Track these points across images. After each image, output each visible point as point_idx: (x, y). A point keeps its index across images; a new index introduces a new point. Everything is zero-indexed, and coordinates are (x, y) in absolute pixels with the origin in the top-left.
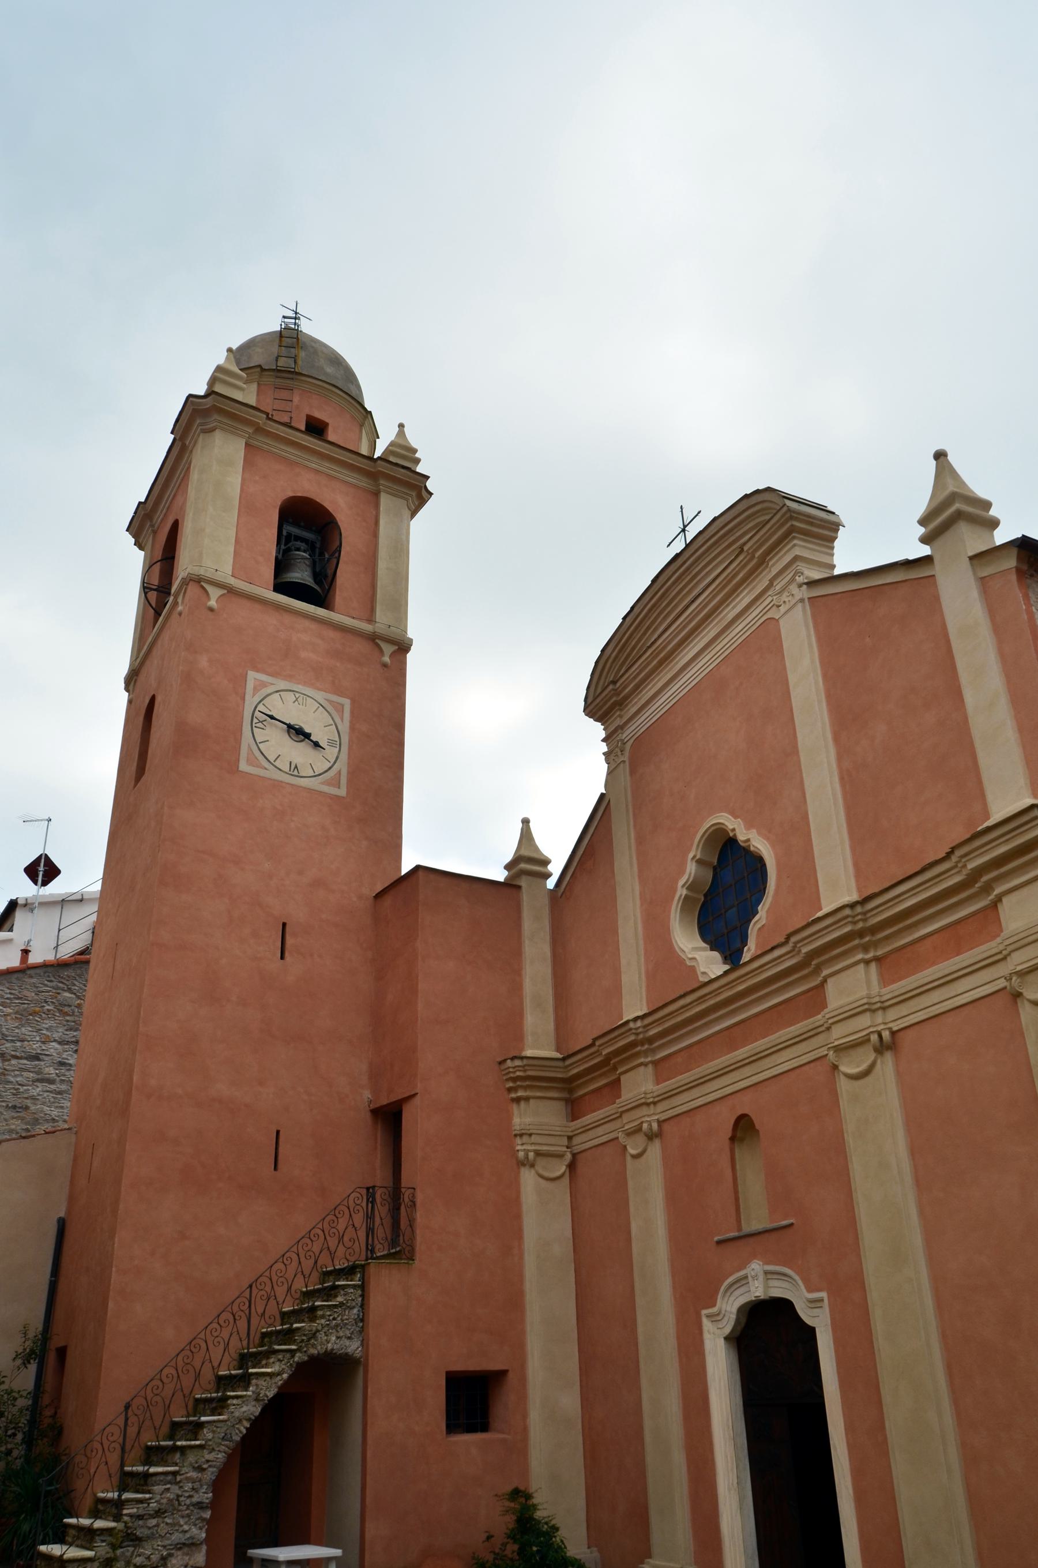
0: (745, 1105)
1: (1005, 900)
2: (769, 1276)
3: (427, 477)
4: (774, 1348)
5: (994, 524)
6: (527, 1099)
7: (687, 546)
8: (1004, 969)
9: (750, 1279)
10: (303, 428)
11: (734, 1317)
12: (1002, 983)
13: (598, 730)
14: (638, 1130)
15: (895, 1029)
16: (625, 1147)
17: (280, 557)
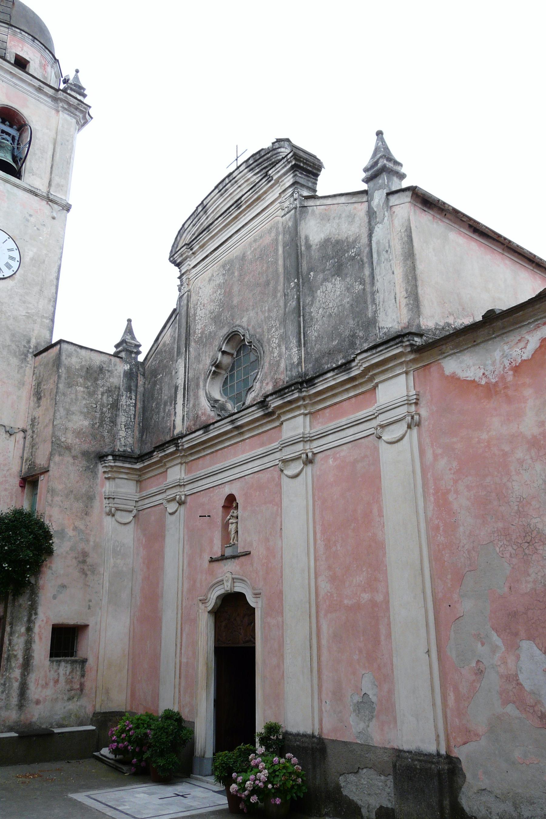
0: (234, 489)
1: (380, 386)
2: (235, 581)
4: (233, 616)
5: (402, 176)
6: (114, 479)
8: (374, 423)
9: (224, 581)
10: (13, 62)
11: (214, 601)
12: (372, 431)
14: (174, 499)
15: (315, 452)
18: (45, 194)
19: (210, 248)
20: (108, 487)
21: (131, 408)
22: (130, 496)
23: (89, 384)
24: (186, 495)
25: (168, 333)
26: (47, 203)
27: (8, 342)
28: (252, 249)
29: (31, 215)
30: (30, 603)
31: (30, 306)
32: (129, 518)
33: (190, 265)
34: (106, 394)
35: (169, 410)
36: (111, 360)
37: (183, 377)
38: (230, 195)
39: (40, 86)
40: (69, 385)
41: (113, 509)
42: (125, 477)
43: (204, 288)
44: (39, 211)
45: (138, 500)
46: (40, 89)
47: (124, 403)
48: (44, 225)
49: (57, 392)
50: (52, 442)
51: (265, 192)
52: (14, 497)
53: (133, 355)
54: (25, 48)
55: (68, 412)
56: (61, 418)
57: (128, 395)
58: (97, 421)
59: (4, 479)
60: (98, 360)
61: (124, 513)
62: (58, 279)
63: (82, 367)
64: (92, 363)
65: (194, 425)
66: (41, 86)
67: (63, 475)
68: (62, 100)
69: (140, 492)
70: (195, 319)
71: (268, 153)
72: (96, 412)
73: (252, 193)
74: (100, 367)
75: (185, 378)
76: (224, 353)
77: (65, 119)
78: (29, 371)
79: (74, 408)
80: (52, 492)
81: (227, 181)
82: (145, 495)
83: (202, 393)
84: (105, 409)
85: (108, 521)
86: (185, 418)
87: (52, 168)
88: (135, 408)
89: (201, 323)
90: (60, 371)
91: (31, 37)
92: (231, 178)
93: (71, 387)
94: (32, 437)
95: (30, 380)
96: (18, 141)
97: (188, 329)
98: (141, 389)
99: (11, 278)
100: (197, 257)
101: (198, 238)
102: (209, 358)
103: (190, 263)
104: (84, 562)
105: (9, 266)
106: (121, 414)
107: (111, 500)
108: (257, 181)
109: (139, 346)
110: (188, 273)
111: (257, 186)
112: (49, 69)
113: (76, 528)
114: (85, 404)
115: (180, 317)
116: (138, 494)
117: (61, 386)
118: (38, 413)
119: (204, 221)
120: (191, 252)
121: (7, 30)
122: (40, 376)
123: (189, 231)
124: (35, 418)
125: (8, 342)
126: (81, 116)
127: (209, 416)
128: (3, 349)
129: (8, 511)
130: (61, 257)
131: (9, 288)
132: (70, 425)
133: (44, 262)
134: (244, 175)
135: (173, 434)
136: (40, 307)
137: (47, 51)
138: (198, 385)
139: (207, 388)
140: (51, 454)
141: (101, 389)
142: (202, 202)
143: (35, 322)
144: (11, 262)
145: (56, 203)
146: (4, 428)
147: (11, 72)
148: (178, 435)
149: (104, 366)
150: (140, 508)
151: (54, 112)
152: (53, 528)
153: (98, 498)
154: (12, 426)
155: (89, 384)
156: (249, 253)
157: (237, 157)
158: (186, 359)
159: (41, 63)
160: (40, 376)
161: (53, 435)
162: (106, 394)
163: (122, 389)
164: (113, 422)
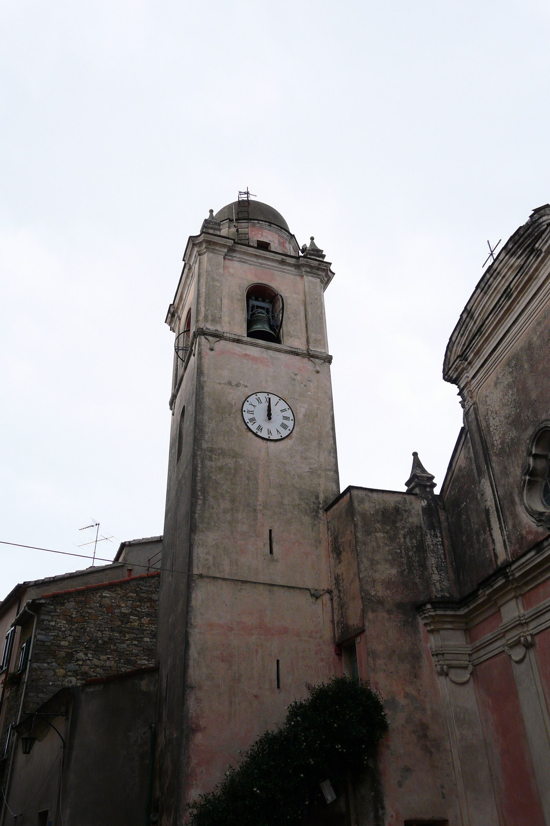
3: (330, 264)
6: (438, 630)
7: (495, 260)
10: (256, 246)
13: (455, 389)
14: (517, 643)
16: (510, 655)
17: (249, 318)
18: (305, 352)
19: (487, 352)
20: (433, 642)
21: (439, 547)
22: (461, 649)
23: (388, 528)
24: (532, 635)
25: (462, 455)
26: (309, 360)
27: (298, 502)
28: (538, 333)
29: (296, 374)
30: (373, 794)
31: (312, 461)
32: (465, 676)
33: (468, 377)
34: (408, 536)
35: (484, 540)
36: (405, 498)
37: (492, 497)
38: (495, 289)
39: (283, 259)
40: (368, 533)
41: (445, 667)
42: (450, 626)
43: (492, 395)
44: (302, 369)
45: (471, 652)
46: (283, 262)
47: (430, 543)
48: (310, 381)
49: (356, 542)
50: (362, 598)
51: (536, 270)
52: (332, 667)
53: (428, 489)
54: (264, 234)
55: (373, 563)
56: (366, 570)
57: (433, 533)
58: (406, 567)
59: (319, 648)
60: (391, 501)
61: (459, 671)
62: (333, 429)
63: (377, 511)
64: (387, 505)
65: (520, 548)
66: (284, 259)
67: (381, 634)
68: (303, 265)
69: (471, 642)
70: (489, 431)
71: (528, 229)
72: (401, 557)
73: (521, 276)
74: (395, 508)
75: (495, 498)
76: (535, 456)
77: (310, 281)
78: (323, 527)
79: (377, 557)
80: (373, 654)
81: (488, 276)
82: (478, 645)
83: (521, 511)
84: (410, 553)
85: (442, 683)
86: (507, 543)
87: (306, 327)
88: (443, 547)
89: (498, 431)
90: (355, 519)
91: (267, 224)
92: (492, 271)
93: (370, 534)
94: (339, 597)
95: (325, 537)
96: (272, 312)
97: (484, 444)
98: (444, 525)
99: (289, 437)
100: (474, 366)
101: (471, 346)
102: (519, 467)
103: (468, 375)
104: (425, 736)
105: (284, 426)
106: (429, 555)
107: (440, 656)
108: (522, 263)
109: (433, 477)
110: (468, 386)
111: (525, 267)
112: (287, 245)
113: (408, 695)
114: (388, 551)
115: (472, 436)
116: (470, 646)
117: (359, 535)
118: (341, 569)
119: (472, 327)
120: (466, 363)
121: (247, 224)
122: (335, 530)
123: (459, 343)
124: (338, 576)
125: (298, 502)
126: (324, 274)
127: (537, 533)
128: (294, 509)
129: (330, 682)
130: (333, 408)
131: (289, 448)
132: (377, 576)
133: (317, 415)
134: (507, 262)
135: (497, 564)
136: (322, 460)
137: (283, 231)
138: (513, 502)
139: (525, 501)
140: (364, 611)
141: (402, 532)
142: (466, 308)
143: (319, 476)
144: (285, 422)
145: (317, 358)
146: (308, 591)
147: (256, 255)
148: (502, 564)
149: (400, 506)
150: (476, 662)
151: (298, 278)
152: (383, 697)
153: (424, 656)
154: (316, 587)
155: (388, 528)
156: (535, 339)
157: (492, 252)
158: (490, 477)
159: (279, 242)
160: (335, 530)
161: (362, 590)
162: (408, 536)
163: (424, 528)
164: (423, 565)
